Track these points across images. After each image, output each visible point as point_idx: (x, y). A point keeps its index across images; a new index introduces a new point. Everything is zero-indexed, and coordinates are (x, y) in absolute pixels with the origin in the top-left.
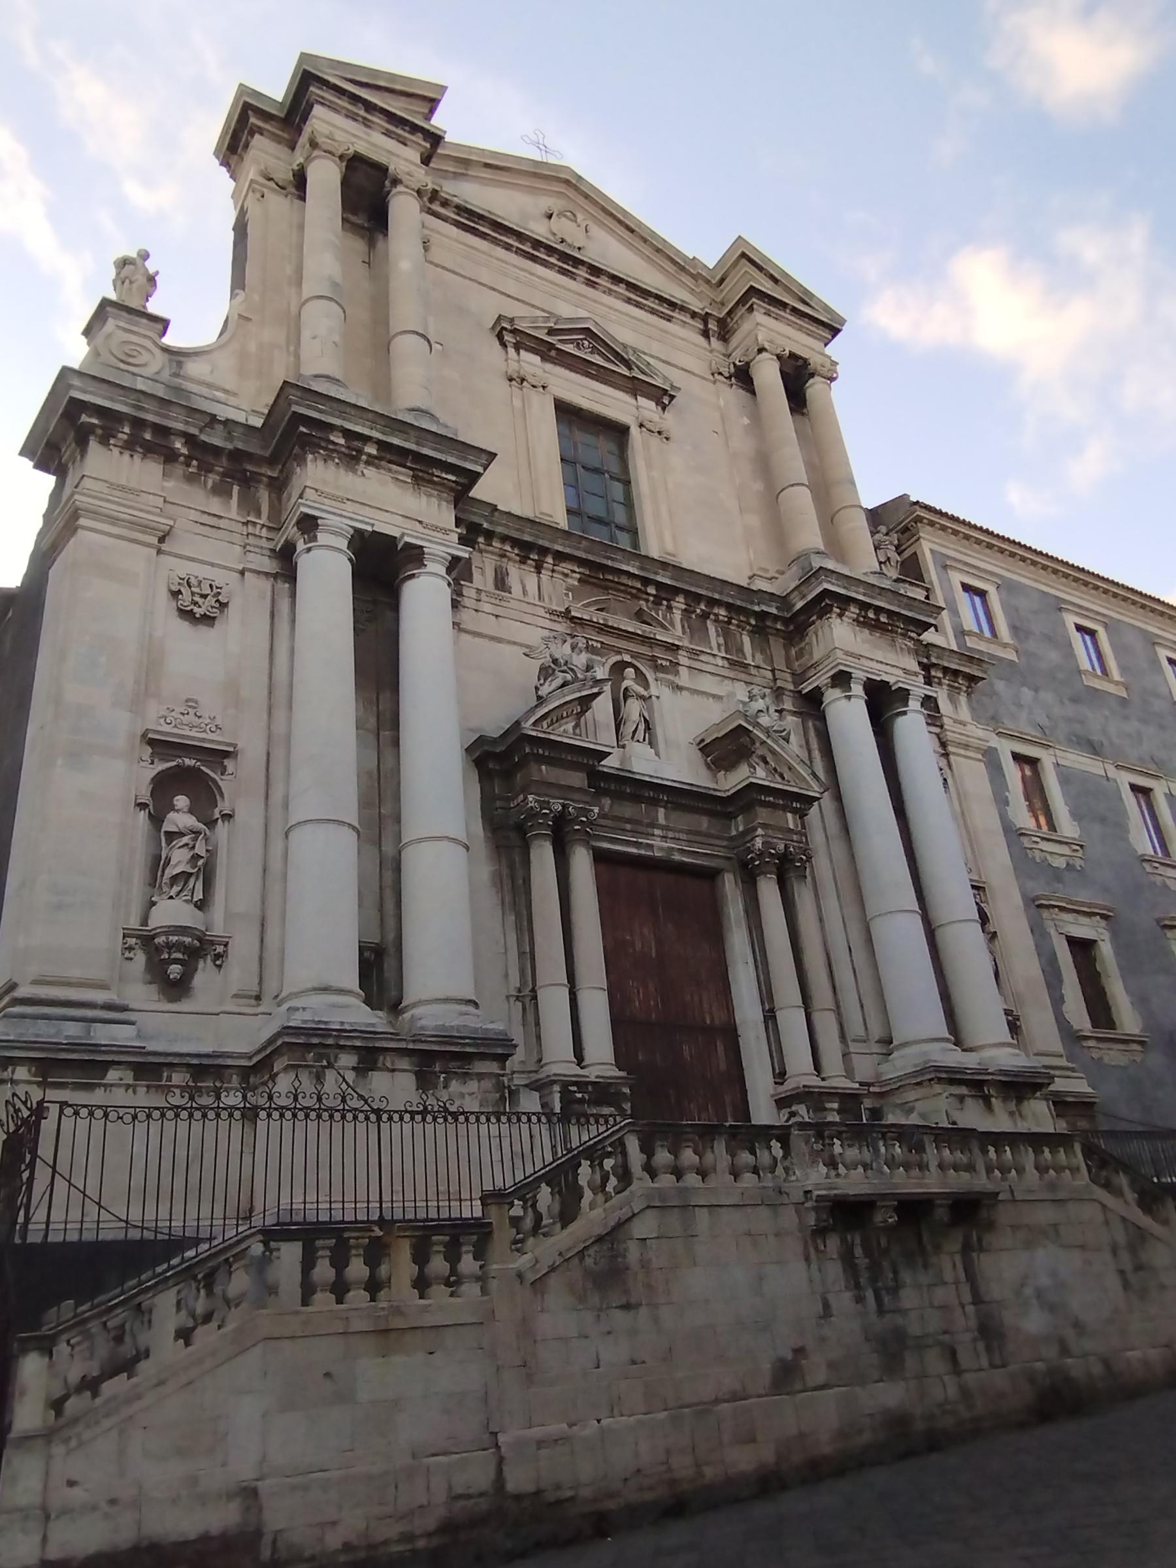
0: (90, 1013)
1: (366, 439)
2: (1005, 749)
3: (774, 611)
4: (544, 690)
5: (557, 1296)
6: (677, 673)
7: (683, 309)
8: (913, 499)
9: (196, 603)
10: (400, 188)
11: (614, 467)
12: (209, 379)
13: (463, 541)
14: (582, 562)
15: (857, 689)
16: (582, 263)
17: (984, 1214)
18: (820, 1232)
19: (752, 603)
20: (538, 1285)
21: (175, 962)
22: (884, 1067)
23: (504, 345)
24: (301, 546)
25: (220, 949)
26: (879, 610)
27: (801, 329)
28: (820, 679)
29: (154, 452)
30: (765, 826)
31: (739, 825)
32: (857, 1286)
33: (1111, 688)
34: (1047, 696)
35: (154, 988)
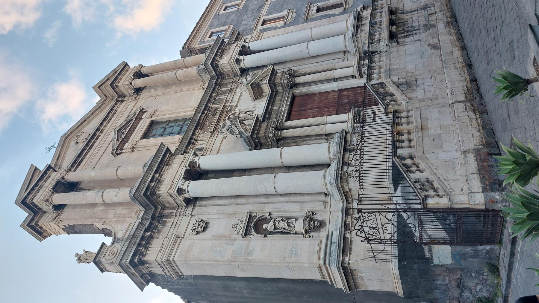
0: (329, 243)
1: (153, 177)
2: (260, 27)
3: (215, 81)
4: (237, 132)
5: (414, 95)
6: (232, 106)
7: (113, 107)
8: (181, 49)
9: (201, 227)
10: (66, 177)
11: (164, 125)
12: (124, 231)
14: (196, 129)
15: (241, 57)
16: (95, 133)
17: (394, 9)
18: (397, 43)
20: (410, 99)
21: (313, 225)
22: (352, 53)
23: (121, 153)
24: (186, 195)
25: (311, 213)
26: (217, 52)
27: (125, 74)
28: (237, 68)
29: (149, 241)
30: (281, 80)
31: (279, 88)
32: (412, 35)
33: (243, 3)
34: (245, 18)
35: (322, 230)
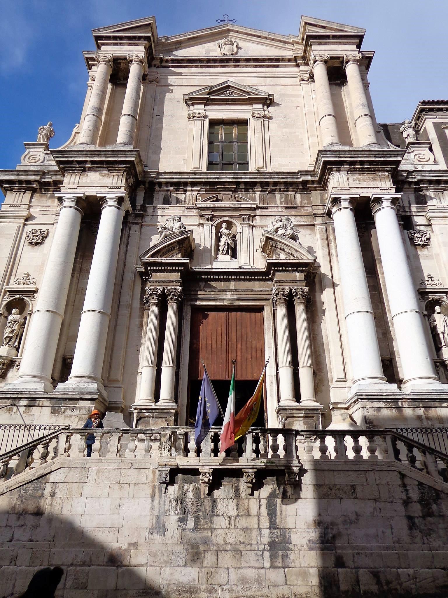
1: (85, 162)
13: (397, 190)
19: (298, 178)
